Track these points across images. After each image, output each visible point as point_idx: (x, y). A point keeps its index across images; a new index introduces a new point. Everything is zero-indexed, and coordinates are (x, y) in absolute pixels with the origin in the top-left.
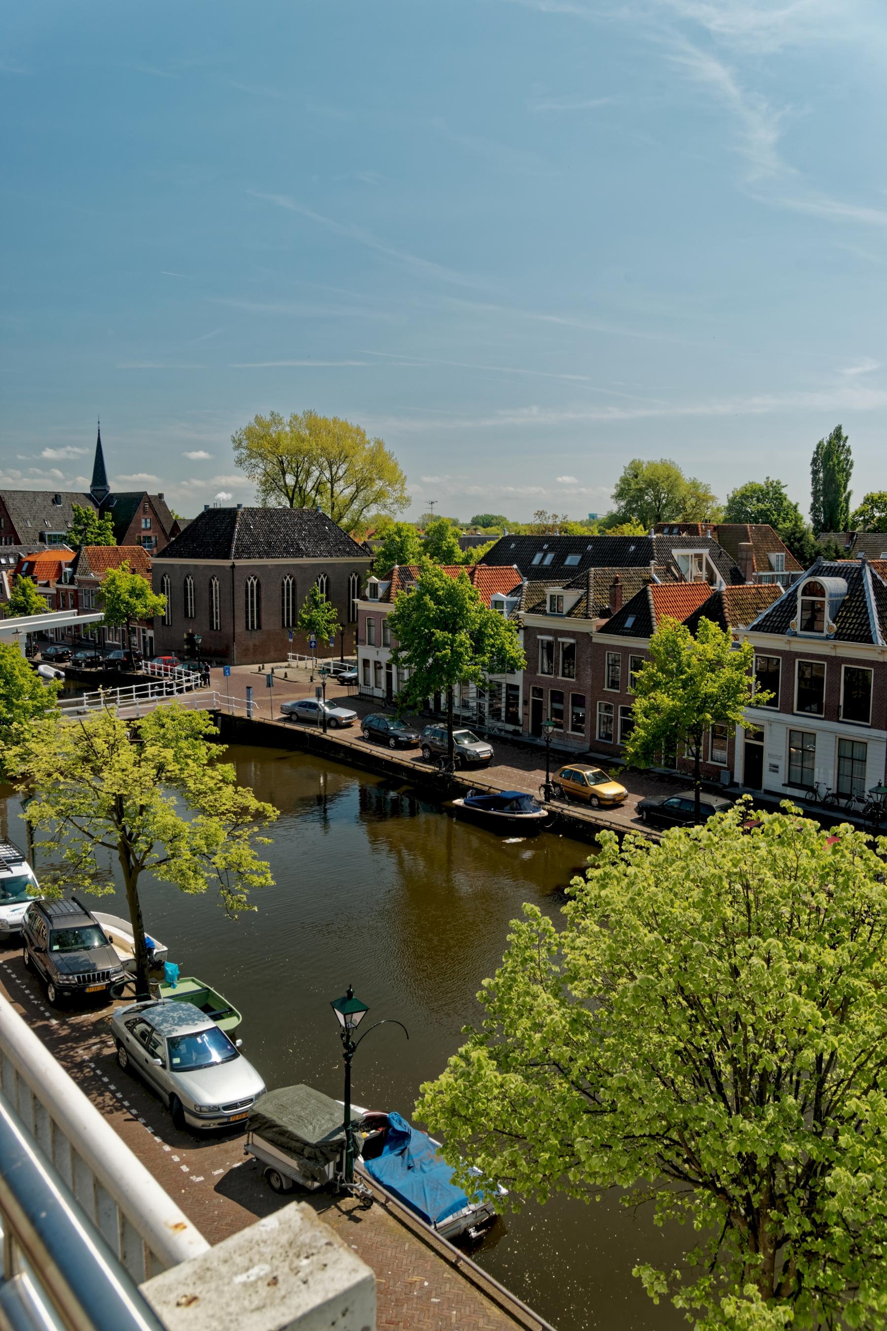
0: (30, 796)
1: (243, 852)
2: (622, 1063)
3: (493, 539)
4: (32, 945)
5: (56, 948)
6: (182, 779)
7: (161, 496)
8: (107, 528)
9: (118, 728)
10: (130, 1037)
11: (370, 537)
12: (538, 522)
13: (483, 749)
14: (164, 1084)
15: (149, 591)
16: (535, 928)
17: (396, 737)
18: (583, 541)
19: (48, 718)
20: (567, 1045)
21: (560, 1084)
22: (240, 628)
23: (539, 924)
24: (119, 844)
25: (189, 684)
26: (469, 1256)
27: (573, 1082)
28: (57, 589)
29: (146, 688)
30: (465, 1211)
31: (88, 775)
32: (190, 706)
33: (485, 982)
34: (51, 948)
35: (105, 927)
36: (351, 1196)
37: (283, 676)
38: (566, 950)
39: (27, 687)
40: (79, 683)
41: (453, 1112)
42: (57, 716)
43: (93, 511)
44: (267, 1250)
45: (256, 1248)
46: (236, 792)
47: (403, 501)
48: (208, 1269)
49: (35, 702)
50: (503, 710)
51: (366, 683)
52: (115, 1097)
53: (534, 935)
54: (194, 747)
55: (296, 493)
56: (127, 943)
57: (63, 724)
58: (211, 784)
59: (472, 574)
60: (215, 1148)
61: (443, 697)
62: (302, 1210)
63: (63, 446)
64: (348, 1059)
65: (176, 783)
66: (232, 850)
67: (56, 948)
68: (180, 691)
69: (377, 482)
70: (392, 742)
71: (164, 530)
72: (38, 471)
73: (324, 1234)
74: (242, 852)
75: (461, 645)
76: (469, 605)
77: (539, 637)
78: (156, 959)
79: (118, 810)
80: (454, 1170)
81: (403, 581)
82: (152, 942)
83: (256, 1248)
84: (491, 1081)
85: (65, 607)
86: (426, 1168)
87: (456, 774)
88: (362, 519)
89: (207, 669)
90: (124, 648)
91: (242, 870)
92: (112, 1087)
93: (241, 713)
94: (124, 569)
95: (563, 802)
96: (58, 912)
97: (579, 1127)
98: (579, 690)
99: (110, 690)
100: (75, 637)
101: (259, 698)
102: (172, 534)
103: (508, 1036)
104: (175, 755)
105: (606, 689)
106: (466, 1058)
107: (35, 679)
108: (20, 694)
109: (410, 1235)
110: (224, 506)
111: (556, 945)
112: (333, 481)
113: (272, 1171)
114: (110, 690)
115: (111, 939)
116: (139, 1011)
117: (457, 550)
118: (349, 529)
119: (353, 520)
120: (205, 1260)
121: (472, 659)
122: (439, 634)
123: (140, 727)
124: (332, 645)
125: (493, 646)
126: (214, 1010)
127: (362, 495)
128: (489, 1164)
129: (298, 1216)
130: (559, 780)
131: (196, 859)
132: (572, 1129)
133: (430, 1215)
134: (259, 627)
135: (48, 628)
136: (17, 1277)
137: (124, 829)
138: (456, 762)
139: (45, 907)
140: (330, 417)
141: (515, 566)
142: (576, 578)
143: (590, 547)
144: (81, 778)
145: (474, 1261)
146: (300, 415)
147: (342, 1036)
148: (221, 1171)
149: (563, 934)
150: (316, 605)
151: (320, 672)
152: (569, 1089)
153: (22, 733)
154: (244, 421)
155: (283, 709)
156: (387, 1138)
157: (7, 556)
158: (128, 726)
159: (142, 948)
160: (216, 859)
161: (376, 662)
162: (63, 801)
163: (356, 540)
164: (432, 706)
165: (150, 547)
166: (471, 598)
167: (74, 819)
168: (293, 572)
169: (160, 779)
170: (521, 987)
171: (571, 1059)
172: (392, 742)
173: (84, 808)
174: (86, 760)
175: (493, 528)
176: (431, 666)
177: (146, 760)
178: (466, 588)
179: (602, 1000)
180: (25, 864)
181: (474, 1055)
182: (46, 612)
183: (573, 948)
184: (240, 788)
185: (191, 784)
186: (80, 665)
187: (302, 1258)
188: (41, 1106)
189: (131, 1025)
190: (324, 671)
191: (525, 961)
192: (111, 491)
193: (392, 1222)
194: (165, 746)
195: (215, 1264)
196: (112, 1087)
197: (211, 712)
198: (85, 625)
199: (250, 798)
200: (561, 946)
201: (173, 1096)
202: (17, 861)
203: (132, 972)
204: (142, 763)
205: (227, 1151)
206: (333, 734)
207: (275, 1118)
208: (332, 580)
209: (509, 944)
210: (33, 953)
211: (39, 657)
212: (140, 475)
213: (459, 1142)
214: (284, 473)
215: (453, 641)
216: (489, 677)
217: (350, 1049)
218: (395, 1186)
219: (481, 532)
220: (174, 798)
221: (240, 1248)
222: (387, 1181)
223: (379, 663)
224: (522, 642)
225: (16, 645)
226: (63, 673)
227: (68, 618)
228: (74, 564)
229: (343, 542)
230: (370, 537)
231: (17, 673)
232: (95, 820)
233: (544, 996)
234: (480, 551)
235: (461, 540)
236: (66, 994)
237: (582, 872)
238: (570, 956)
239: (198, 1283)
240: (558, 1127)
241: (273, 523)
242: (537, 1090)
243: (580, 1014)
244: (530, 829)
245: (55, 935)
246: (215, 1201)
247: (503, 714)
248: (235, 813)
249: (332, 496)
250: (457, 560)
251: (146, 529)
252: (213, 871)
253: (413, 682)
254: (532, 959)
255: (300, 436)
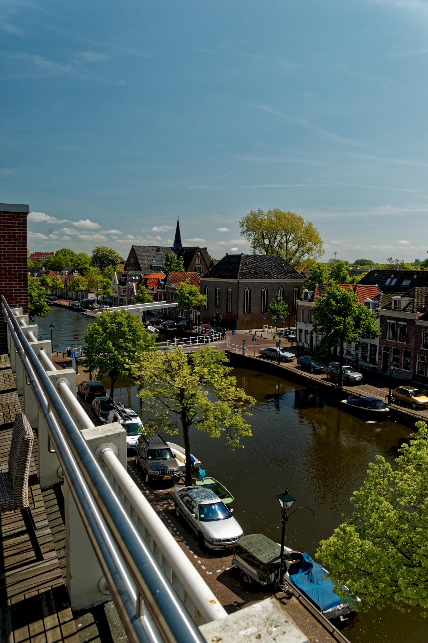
0: (141, 387)
1: (238, 419)
2: (425, 541)
3: (366, 272)
4: (140, 455)
5: (150, 457)
6: (211, 383)
7: (205, 249)
8: (181, 264)
9: (183, 357)
10: (181, 502)
11: (304, 269)
12: (389, 263)
13: (357, 376)
14: (196, 526)
15: (199, 293)
16: (382, 468)
17: (314, 368)
18: (412, 273)
19: (151, 351)
20: (396, 529)
21: (392, 549)
22: (241, 312)
23: (384, 466)
24: (181, 412)
25: (216, 338)
26: (339, 630)
27: (398, 549)
28: (157, 291)
29: (196, 339)
30: (338, 607)
31: (168, 379)
32: (216, 348)
33: (355, 493)
34: (148, 457)
35: (172, 449)
36: (282, 591)
37: (260, 336)
38: (397, 481)
39: (142, 336)
40: (165, 336)
41: (336, 556)
42: (155, 350)
43: (174, 255)
44: (256, 620)
45: (251, 618)
46: (236, 390)
47: (321, 252)
48: (227, 625)
49: (145, 343)
50: (368, 357)
51: (300, 341)
52: (173, 530)
53: (381, 471)
54: (218, 368)
55: (269, 248)
56: (182, 458)
57: (159, 354)
58: (225, 386)
59: (355, 289)
60: (218, 559)
61: (338, 350)
62: (273, 603)
63: (162, 225)
64: (284, 524)
65: (207, 385)
66: (233, 418)
67: (150, 457)
68: (212, 341)
69: (309, 243)
70: (312, 370)
71: (206, 265)
72: (150, 237)
73: (284, 616)
74: (238, 419)
75: (349, 323)
76: (353, 304)
77: (388, 321)
78: (195, 467)
79: (181, 395)
80: (335, 586)
81: (320, 291)
82: (193, 459)
83: (250, 618)
84: (356, 543)
85: (161, 300)
86: (320, 583)
87: (344, 387)
88: (301, 261)
89: (225, 331)
90: (186, 319)
91: (237, 428)
92: (172, 525)
93: (240, 353)
94: (187, 283)
95: (398, 405)
96: (152, 441)
97: (401, 572)
98: (408, 349)
99: (180, 339)
100: (164, 314)
101: (248, 346)
102: (210, 267)
103: (365, 521)
104: (208, 371)
105: (422, 348)
106: (344, 530)
107: (146, 333)
108: (139, 339)
109: (310, 615)
110: (235, 254)
111: (392, 477)
112: (287, 242)
113: (245, 574)
114: (180, 339)
115: (175, 455)
116: (186, 491)
117: (348, 277)
118: (294, 265)
119: (296, 261)
120: (226, 621)
121: (353, 331)
122: (337, 318)
123: (193, 357)
124: (284, 322)
125: (364, 325)
126: (220, 494)
127: (301, 249)
128: (353, 585)
129: (272, 605)
130: (395, 393)
131: (216, 421)
132: (397, 573)
133: (321, 607)
134: (250, 312)
135: (153, 309)
136: (142, 617)
137: (183, 405)
138: (344, 381)
139: (146, 438)
140: (286, 211)
141: (377, 285)
142: (407, 292)
143: (415, 276)
144: (165, 379)
145: (342, 633)
146: (272, 210)
147: (282, 512)
148: (220, 571)
149: (396, 472)
150: (278, 302)
151: (278, 335)
152: (396, 552)
153: (139, 357)
154: (245, 213)
155: (260, 352)
156: (301, 566)
157: (135, 276)
158: (187, 356)
159: (189, 461)
160: (225, 422)
161: (306, 331)
162: (156, 390)
163: (298, 271)
164: (332, 353)
165: (200, 272)
166: (354, 301)
167: (161, 399)
168: (267, 286)
169: (201, 382)
170: (374, 497)
171: (398, 537)
172: (312, 370)
173: (166, 393)
174: (167, 371)
175: (366, 266)
176: (333, 333)
177: (195, 373)
178: (351, 294)
179: (415, 508)
180: (138, 418)
181: (348, 529)
182: (151, 302)
183: (401, 480)
184: (238, 389)
185: (215, 385)
186: (166, 327)
187: (273, 627)
188: (149, 534)
189: (182, 497)
190: (280, 334)
191: (376, 484)
192: (183, 246)
193: (301, 607)
194: (204, 367)
195: (231, 623)
196: (172, 525)
197: (226, 351)
198: (169, 308)
199: (243, 393)
200: (395, 478)
201: (200, 532)
202: (134, 416)
203: (184, 472)
204: (193, 374)
205: (223, 562)
206: (283, 365)
207: (247, 548)
208: (285, 290)
209: (368, 475)
210: (140, 459)
211: (148, 322)
212: (196, 239)
213: (338, 572)
214: (264, 238)
215: (345, 322)
216: (362, 340)
217: (285, 519)
218: (304, 589)
219: (359, 268)
220: (207, 391)
221: (243, 617)
222: (300, 586)
223: (307, 331)
224: (379, 323)
225: (138, 317)
226: (158, 330)
227: (161, 305)
228: (165, 280)
229: (291, 272)
230: (304, 269)
231: (138, 329)
232: (170, 400)
233: (386, 503)
234: (359, 278)
235: (349, 271)
236: (154, 479)
237: (407, 441)
238: (400, 484)
239: (222, 631)
240: (389, 569)
241: (258, 262)
242: (379, 550)
243: (404, 514)
244: (380, 417)
245: (150, 451)
246: (217, 585)
247: (368, 359)
248: (235, 400)
249: (286, 250)
250: (347, 281)
251: (198, 264)
252: (224, 427)
253: (324, 341)
254: (380, 484)
255: (272, 221)
